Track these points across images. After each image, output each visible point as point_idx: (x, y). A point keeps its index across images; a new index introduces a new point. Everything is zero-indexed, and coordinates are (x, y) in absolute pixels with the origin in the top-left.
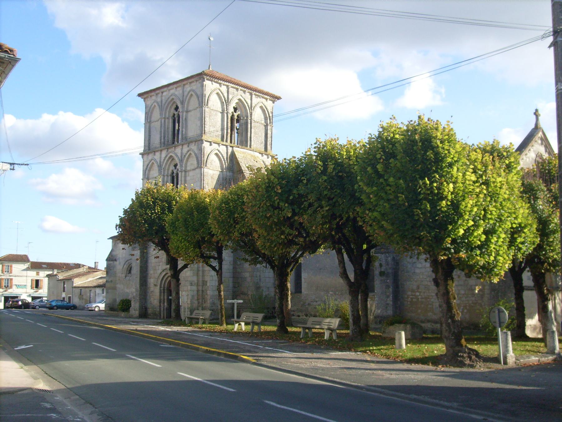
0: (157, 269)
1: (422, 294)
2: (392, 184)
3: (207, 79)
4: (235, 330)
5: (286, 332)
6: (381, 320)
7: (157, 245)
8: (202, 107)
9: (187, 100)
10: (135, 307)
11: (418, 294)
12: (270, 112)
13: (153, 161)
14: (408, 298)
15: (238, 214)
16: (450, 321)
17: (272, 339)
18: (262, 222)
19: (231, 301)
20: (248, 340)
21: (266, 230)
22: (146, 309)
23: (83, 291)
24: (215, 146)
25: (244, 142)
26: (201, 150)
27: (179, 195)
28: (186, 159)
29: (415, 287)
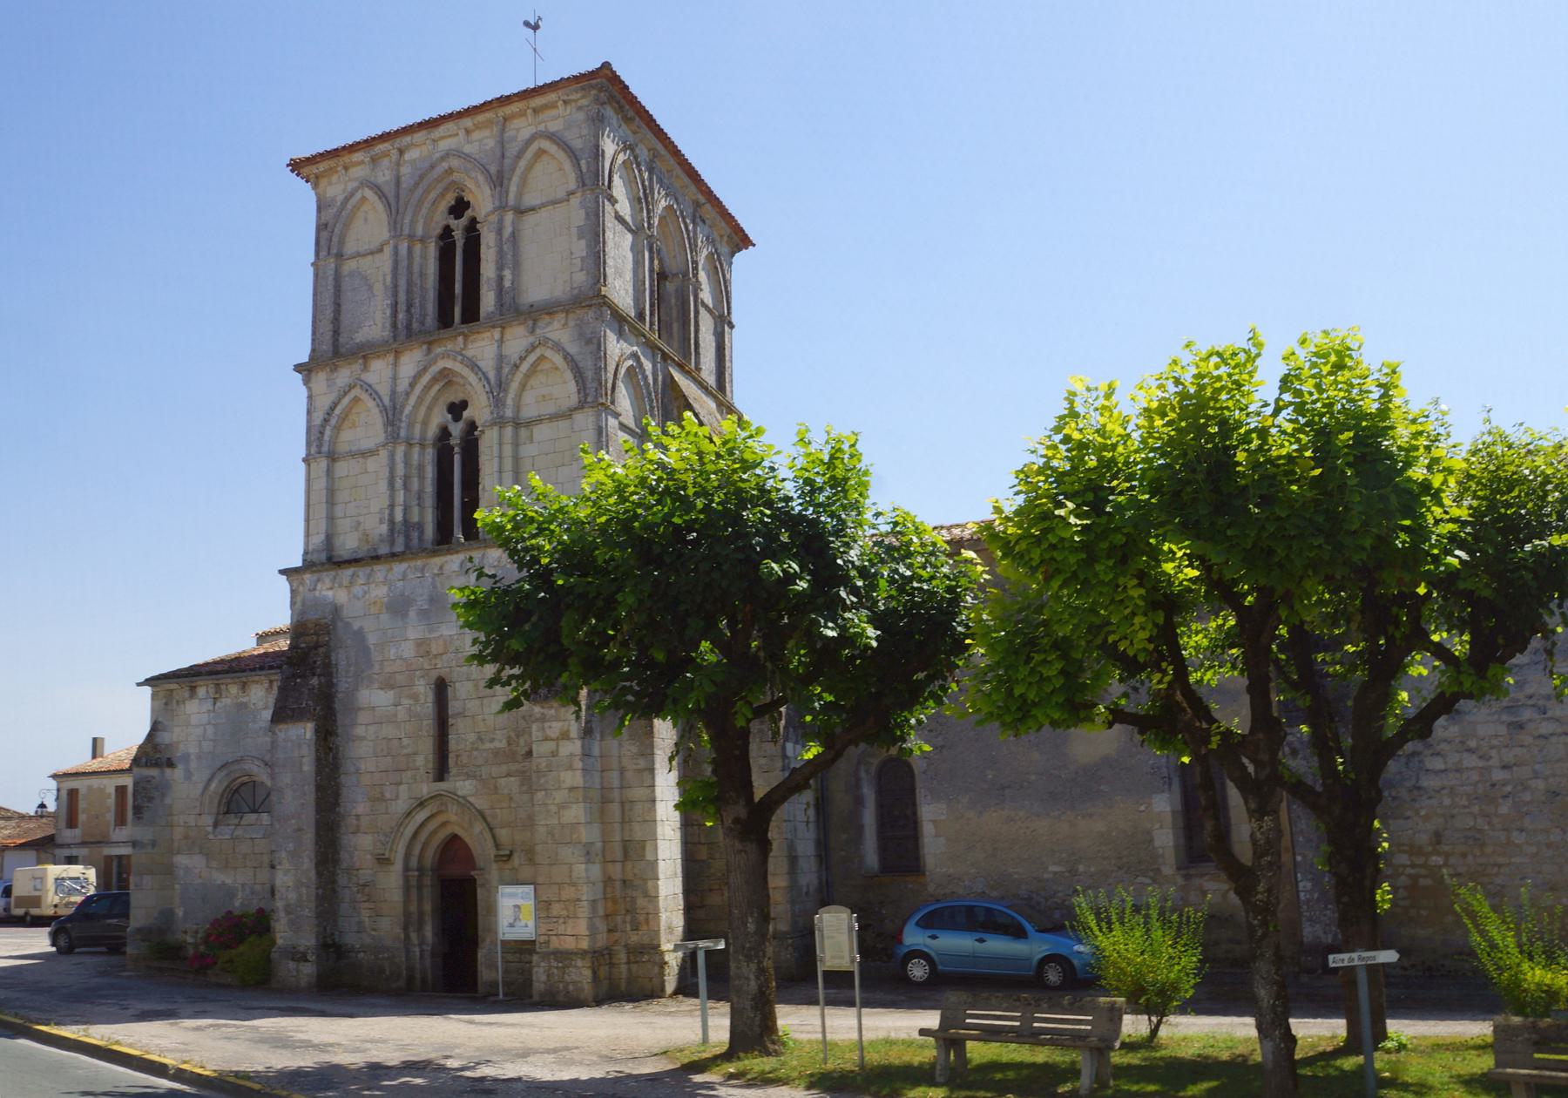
0: (388, 795)
1: (1452, 860)
9: (518, 172)
11: (1436, 860)
13: (356, 392)
28: (519, 377)
29: (1423, 839)
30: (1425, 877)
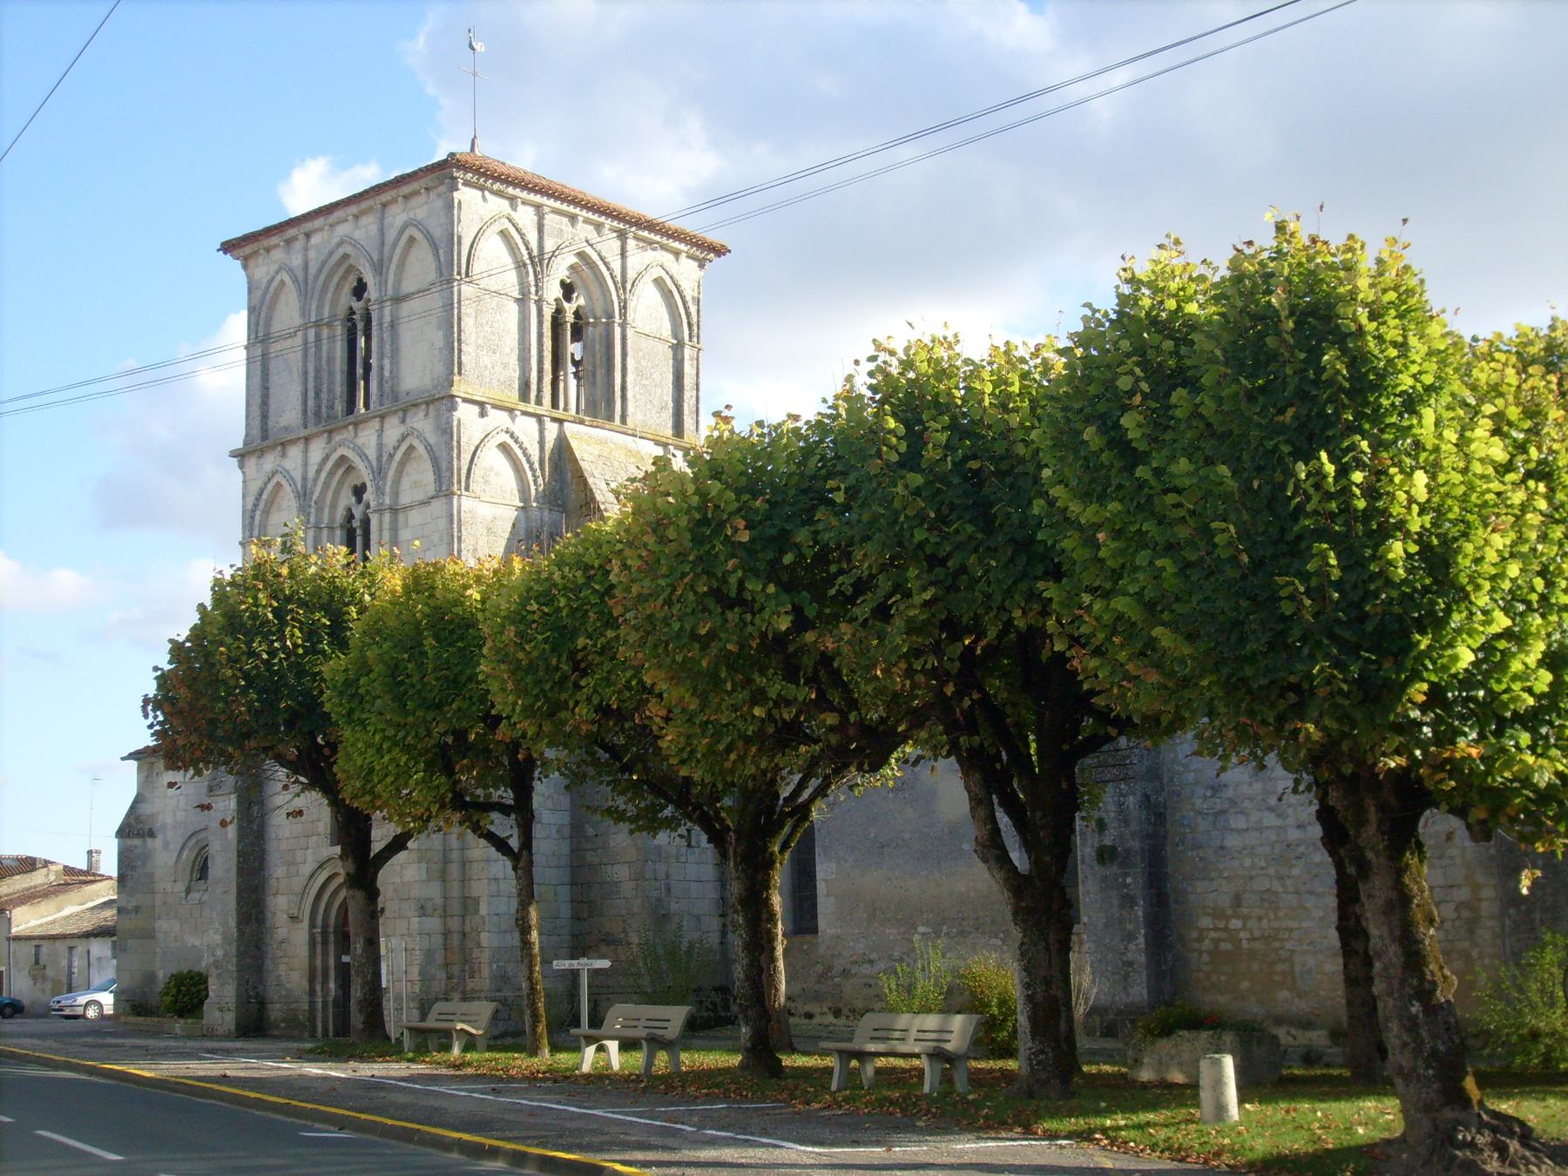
0: (299, 859)
1: (1250, 924)
2: (1187, 482)
3: (467, 184)
4: (586, 1068)
5: (777, 1070)
6: (1111, 1023)
7: (295, 767)
8: (450, 281)
10: (222, 998)
11: (1235, 923)
12: (689, 298)
13: (278, 478)
14: (1200, 939)
15: (589, 637)
16: (1415, 1008)
17: (725, 1097)
18: (679, 658)
19: (566, 964)
20: (636, 1103)
21: (695, 688)
22: (262, 1004)
23: (44, 950)
24: (497, 418)
25: (603, 403)
26: (447, 431)
27: (373, 582)
28: (394, 465)
29: (1225, 901)
30: (1224, 941)
